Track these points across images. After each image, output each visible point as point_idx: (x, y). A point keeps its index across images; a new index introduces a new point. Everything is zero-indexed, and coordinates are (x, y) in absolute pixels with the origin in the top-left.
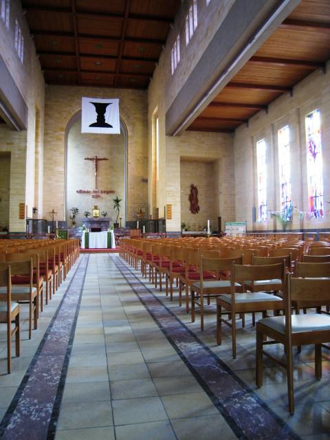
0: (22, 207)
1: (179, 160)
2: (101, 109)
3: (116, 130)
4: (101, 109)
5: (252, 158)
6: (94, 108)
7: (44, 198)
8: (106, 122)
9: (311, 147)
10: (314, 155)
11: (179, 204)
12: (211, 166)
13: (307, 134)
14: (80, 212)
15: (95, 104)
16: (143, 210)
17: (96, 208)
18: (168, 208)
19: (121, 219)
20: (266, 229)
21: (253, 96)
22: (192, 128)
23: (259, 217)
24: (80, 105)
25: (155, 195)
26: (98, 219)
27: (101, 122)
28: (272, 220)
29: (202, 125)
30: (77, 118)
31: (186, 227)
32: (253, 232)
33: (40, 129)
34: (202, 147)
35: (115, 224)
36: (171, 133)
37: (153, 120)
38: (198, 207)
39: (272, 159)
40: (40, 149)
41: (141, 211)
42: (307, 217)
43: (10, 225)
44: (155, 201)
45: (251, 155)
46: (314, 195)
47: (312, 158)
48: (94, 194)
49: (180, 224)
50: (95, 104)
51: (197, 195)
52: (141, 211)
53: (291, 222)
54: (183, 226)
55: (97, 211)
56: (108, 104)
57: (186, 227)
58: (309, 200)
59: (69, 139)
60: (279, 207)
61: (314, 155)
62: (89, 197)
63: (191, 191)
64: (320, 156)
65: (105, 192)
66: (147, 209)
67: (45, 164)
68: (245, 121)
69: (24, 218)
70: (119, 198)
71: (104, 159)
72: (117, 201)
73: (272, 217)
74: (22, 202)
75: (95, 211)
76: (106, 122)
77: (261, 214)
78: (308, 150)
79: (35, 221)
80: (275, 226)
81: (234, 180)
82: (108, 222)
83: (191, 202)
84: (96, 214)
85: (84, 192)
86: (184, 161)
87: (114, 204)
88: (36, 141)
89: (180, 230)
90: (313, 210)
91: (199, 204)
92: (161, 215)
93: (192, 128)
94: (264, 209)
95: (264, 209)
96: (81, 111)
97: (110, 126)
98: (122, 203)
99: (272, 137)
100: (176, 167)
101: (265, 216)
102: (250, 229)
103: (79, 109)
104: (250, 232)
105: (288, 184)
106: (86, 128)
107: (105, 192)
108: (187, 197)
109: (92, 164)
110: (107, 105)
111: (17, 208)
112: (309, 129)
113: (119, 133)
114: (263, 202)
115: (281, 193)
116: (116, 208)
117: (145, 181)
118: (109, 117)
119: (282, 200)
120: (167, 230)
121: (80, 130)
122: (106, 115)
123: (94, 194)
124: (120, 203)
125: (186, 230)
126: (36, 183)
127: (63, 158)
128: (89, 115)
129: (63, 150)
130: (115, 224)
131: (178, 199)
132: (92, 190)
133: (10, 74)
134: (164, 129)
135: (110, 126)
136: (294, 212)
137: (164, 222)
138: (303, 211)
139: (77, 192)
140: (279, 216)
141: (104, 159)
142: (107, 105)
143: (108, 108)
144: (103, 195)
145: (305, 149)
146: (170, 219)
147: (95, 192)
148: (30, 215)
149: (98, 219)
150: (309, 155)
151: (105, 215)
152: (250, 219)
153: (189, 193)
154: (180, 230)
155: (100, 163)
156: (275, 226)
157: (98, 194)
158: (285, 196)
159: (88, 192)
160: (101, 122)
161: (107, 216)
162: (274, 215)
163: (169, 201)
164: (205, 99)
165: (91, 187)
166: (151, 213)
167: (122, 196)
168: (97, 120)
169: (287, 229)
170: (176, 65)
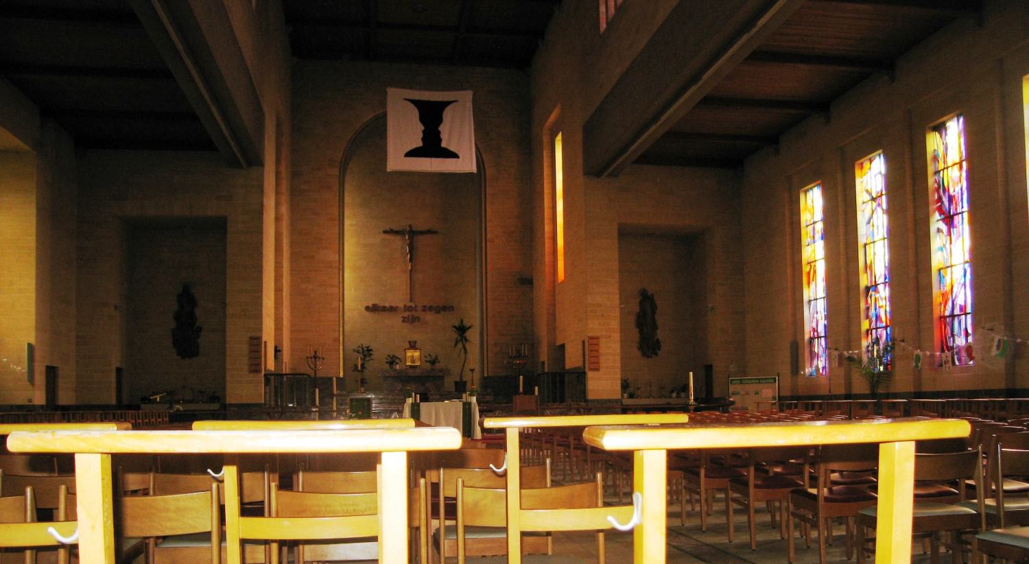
0: (256, 343)
1: (616, 234)
2: (431, 115)
3: (466, 163)
4: (431, 115)
5: (788, 229)
6: (415, 113)
7: (293, 325)
8: (443, 145)
9: (940, 200)
10: (949, 220)
11: (616, 336)
12: (687, 247)
13: (931, 169)
14: (375, 355)
15: (416, 103)
16: (525, 350)
17: (413, 346)
18: (591, 346)
19: (472, 370)
20: (824, 392)
21: (790, 81)
22: (645, 159)
23: (807, 365)
24: (383, 104)
25: (552, 316)
26: (418, 371)
27: (432, 146)
28: (841, 372)
29: (677, 153)
30: (376, 132)
31: (631, 389)
32: (793, 398)
33: (283, 163)
34: (669, 202)
35: (456, 383)
36: (594, 166)
37: (546, 139)
38: (658, 341)
39: (841, 231)
40: (284, 209)
41: (518, 351)
42: (931, 364)
43: (229, 386)
44: (552, 329)
45: (787, 221)
46: (947, 313)
47: (944, 227)
48: (406, 314)
49: (619, 383)
50: (416, 103)
51: (654, 312)
52: (518, 351)
53: (888, 374)
54: (625, 386)
55: (417, 354)
56: (450, 103)
57: (631, 389)
58: (936, 323)
59: (347, 186)
60: (860, 340)
61: (949, 220)
62: (396, 321)
63: (641, 303)
64: (963, 226)
65: (431, 308)
66: (534, 345)
67: (293, 244)
68: (771, 139)
69: (259, 371)
70: (467, 323)
71: (429, 232)
72: (462, 330)
73: (840, 364)
74: (253, 334)
75: (409, 354)
76: (443, 145)
77: (812, 360)
78: (933, 207)
79: (279, 376)
80: (849, 384)
81: (532, 291)
82: (442, 378)
83: (641, 332)
84: (413, 361)
85: (384, 309)
86: (627, 234)
87: (455, 336)
88: (278, 193)
89: (619, 397)
90: (945, 347)
91: (660, 335)
92: (572, 359)
93: (645, 159)
94: (820, 346)
95: (820, 346)
96: (385, 115)
97: (454, 155)
98: (474, 335)
99: (839, 176)
100: (608, 253)
101: (821, 363)
102: (786, 392)
103: (367, 116)
104: (786, 398)
105: (881, 287)
106: (397, 161)
107: (431, 308)
108: (632, 319)
109: (399, 243)
110: (445, 105)
111: (245, 348)
112: (935, 158)
113: (474, 170)
114: (815, 330)
115: (863, 306)
116: (460, 345)
117: (527, 282)
118: (450, 134)
119: (865, 325)
120: (590, 396)
121: (383, 159)
122: (444, 130)
123: (406, 314)
124: (468, 334)
125: (631, 396)
126: (278, 290)
127: (336, 230)
128: (403, 132)
129: (336, 211)
130: (456, 383)
131: (615, 324)
132: (401, 305)
133: (232, 30)
134: (580, 160)
135: (454, 155)
136: (898, 351)
137: (580, 375)
138: (919, 348)
139: (367, 308)
140: (860, 361)
141: (429, 232)
142: (445, 105)
143: (448, 114)
144: (429, 317)
145: (927, 204)
146: (597, 369)
147: (407, 308)
148: (271, 365)
149: (418, 371)
150: (936, 223)
151: (433, 362)
152: (786, 370)
153: (638, 310)
154: (619, 397)
155: (422, 241)
156: (849, 384)
157: (416, 314)
158: (872, 312)
159: (392, 309)
160: (432, 146)
161: (437, 364)
162: (850, 359)
163: (594, 327)
164: (694, 88)
165: (398, 298)
166: (544, 355)
167: (473, 318)
168: (423, 139)
169: (880, 391)
170: (612, 11)
